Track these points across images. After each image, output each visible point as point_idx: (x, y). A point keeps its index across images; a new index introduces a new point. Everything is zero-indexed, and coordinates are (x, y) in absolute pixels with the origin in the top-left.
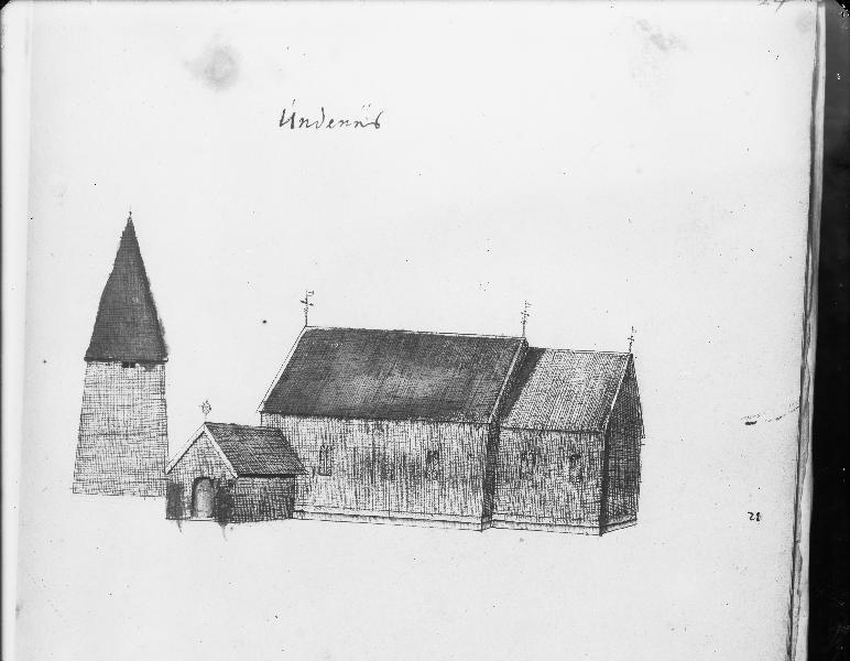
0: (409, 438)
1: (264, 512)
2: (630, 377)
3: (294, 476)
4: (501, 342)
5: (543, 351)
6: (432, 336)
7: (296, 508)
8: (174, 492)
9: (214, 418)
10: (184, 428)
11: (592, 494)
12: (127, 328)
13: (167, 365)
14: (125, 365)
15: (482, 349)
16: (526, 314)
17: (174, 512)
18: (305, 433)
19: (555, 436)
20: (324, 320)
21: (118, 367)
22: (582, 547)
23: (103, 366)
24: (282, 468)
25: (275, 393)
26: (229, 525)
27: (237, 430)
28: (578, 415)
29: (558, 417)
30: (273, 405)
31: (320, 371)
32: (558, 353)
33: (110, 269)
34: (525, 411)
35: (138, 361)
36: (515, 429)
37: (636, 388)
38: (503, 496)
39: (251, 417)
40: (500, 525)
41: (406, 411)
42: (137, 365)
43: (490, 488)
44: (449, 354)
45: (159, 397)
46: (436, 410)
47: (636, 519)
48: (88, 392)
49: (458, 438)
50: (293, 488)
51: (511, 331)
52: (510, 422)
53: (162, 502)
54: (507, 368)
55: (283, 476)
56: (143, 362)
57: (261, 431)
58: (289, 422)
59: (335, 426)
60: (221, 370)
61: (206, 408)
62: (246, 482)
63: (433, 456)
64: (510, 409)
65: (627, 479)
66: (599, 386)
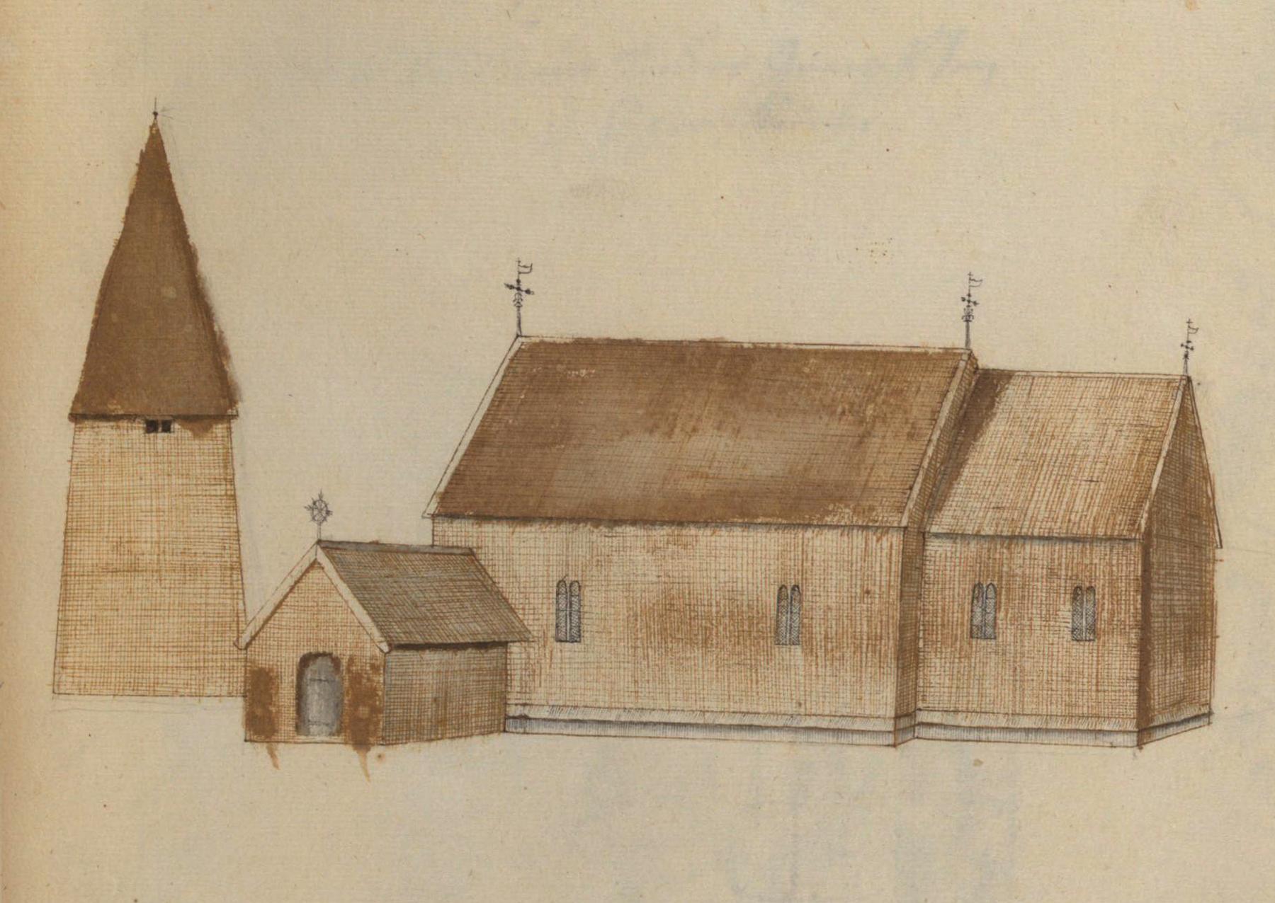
0: (739, 560)
1: (442, 723)
2: (1187, 425)
3: (504, 644)
4: (920, 359)
5: (1007, 376)
6: (779, 350)
7: (514, 711)
8: (258, 688)
9: (335, 530)
10: (276, 548)
11: (1120, 661)
12: (157, 352)
13: (234, 424)
14: (152, 427)
15: (879, 373)
16: (969, 300)
17: (260, 725)
18: (525, 557)
19: (1039, 549)
20: (551, 321)
21: (136, 432)
22: (67, 412)
23: (106, 429)
24: (477, 629)
25: (458, 477)
26: (375, 751)
27: (380, 549)
28: (1084, 505)
29: (1042, 511)
30: (462, 497)
31: (556, 422)
32: (1027, 375)
33: (113, 228)
34: (976, 498)
35: (176, 418)
36: (951, 536)
37: (1200, 444)
38: (938, 675)
39: (409, 525)
40: (932, 732)
41: (735, 507)
42: (176, 426)
43: (909, 659)
44: (818, 386)
45: (220, 490)
46: (797, 503)
47: (1210, 714)
48: (78, 484)
49: (842, 563)
50: (503, 673)
51: (939, 333)
52: (943, 521)
53: (235, 710)
54: (936, 412)
55: (481, 646)
56: (188, 419)
57: (437, 553)
58: (495, 540)
59: (586, 539)
60: (350, 428)
61: (320, 510)
62: (401, 661)
63: (790, 595)
64: (945, 497)
65: (1190, 632)
66: (1125, 444)
